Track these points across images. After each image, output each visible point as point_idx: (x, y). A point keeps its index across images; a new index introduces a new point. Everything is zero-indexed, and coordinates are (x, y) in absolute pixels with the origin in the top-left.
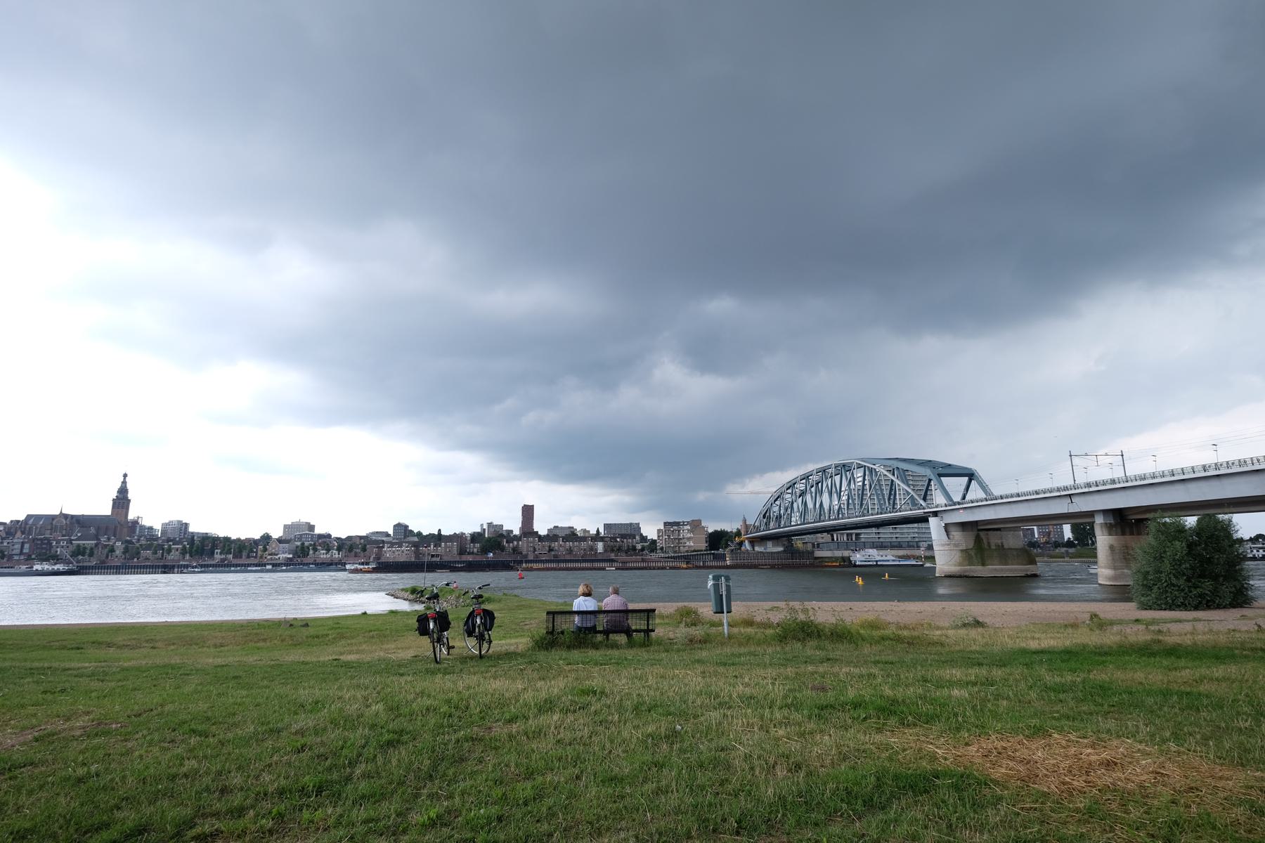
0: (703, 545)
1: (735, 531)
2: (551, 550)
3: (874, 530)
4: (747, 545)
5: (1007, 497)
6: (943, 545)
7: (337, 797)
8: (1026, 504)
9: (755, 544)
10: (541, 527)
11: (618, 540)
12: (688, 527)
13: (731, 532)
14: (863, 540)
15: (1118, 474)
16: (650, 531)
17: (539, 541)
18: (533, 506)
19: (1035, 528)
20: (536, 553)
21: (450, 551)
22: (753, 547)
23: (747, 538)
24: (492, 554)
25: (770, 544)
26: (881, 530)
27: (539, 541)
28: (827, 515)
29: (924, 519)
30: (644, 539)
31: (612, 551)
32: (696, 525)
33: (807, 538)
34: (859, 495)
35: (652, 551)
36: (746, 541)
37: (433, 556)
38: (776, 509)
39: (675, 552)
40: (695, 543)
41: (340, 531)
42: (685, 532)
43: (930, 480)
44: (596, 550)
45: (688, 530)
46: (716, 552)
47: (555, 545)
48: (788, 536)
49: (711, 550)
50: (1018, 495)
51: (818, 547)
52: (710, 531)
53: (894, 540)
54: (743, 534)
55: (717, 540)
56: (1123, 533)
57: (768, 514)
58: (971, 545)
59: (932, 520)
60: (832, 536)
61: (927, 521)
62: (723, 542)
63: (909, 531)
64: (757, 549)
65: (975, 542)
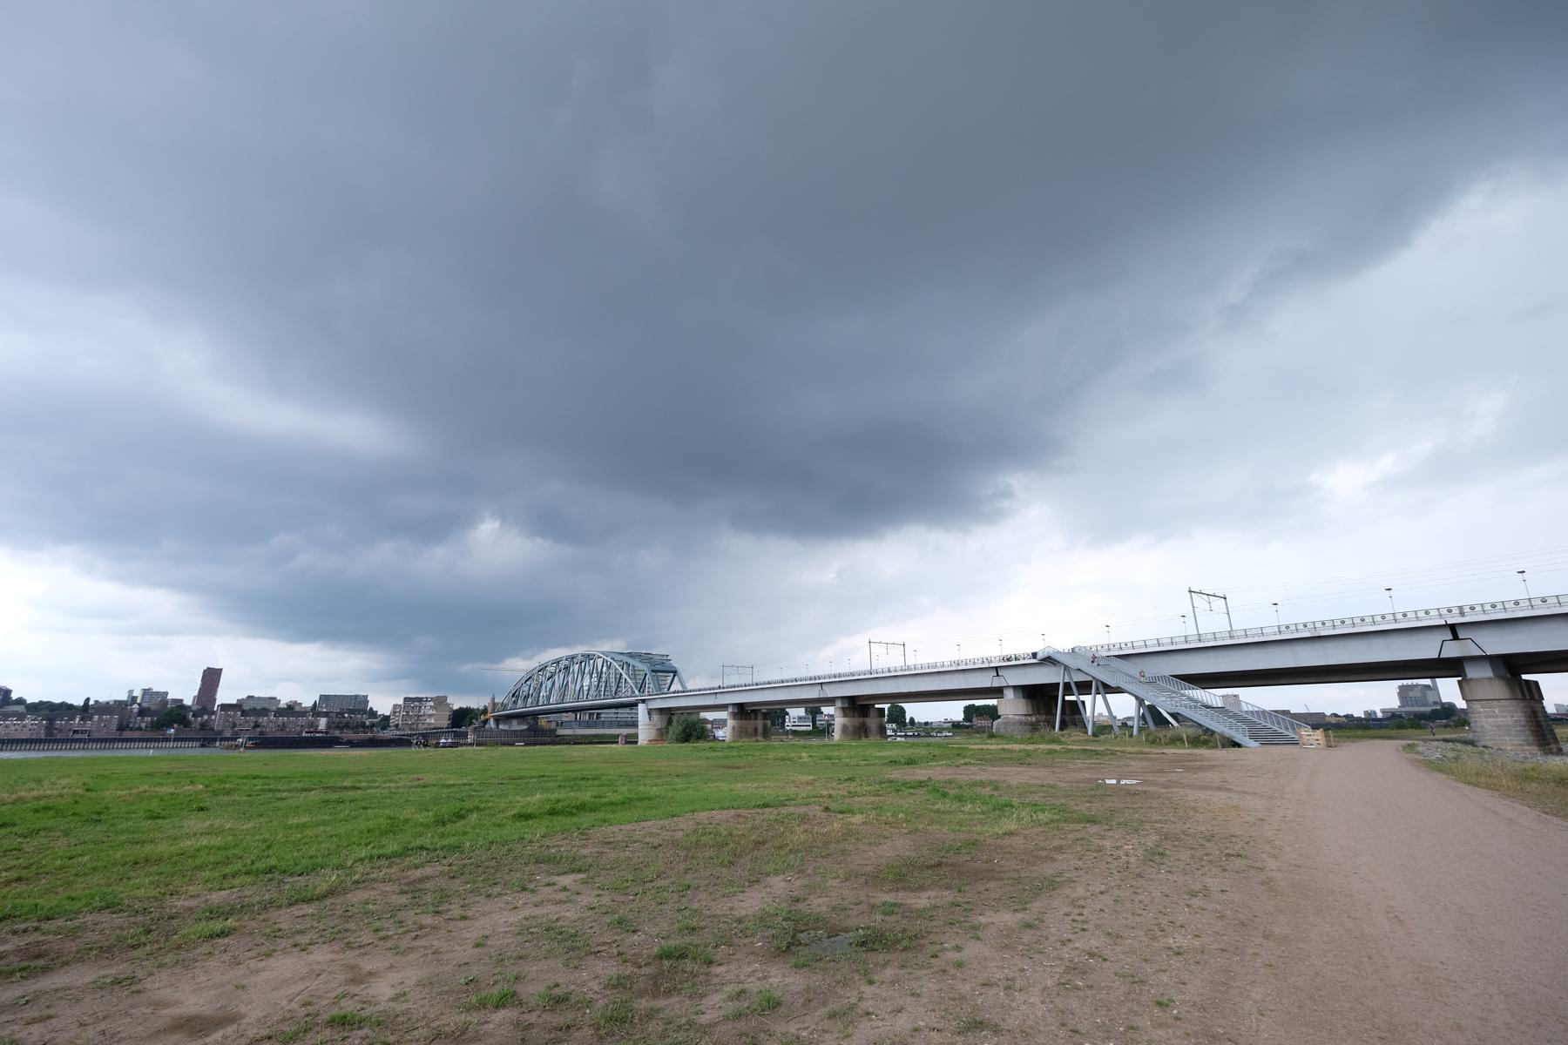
0: (445, 723)
1: (481, 708)
2: (257, 725)
3: (613, 710)
4: (492, 723)
5: (738, 687)
6: (645, 725)
7: (63, 962)
8: (760, 692)
9: (500, 722)
10: (226, 694)
11: (346, 715)
12: (432, 704)
13: (478, 709)
14: (602, 719)
15: (898, 663)
16: (383, 703)
17: (242, 716)
18: (221, 670)
20: (236, 729)
21: (105, 726)
22: (498, 725)
23: (493, 716)
25: (515, 722)
26: (619, 711)
27: (242, 716)
28: (585, 697)
29: (634, 705)
30: (373, 714)
31: (337, 727)
32: (440, 702)
33: (552, 716)
34: (616, 678)
35: (384, 728)
36: (492, 719)
37: (75, 732)
38: (526, 689)
39: (413, 730)
40: (434, 719)
41: (31, 699)
42: (428, 709)
43: (646, 675)
44: (317, 726)
45: (431, 707)
46: (458, 730)
47: (263, 720)
48: (535, 715)
49: (452, 727)
50: (769, 683)
51: (561, 725)
52: (455, 708)
53: (629, 719)
54: (489, 710)
55: (461, 718)
57: (517, 693)
59: (641, 706)
60: (576, 715)
61: (637, 706)
62: (468, 719)
63: (624, 713)
64: (501, 727)
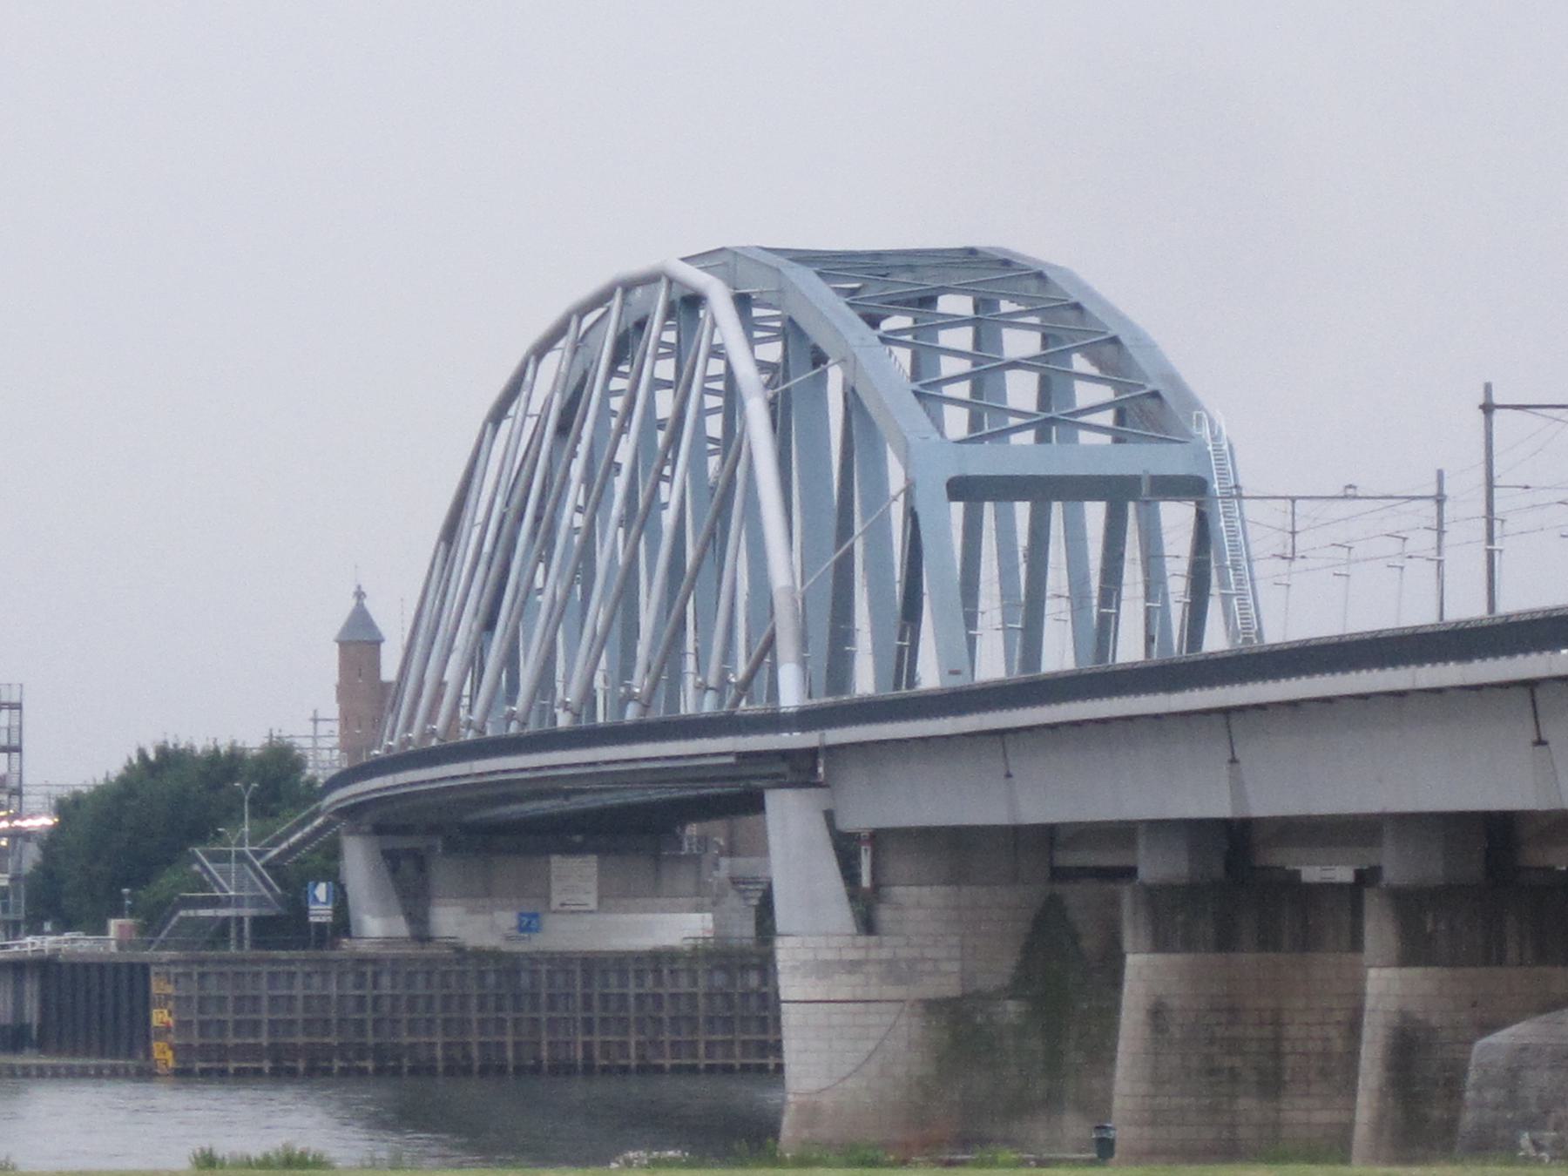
9: (443, 872)
19: (197, 850)
24: (1443, 928)
56: (1225, 942)
58: (999, 968)
65: (1028, 950)
